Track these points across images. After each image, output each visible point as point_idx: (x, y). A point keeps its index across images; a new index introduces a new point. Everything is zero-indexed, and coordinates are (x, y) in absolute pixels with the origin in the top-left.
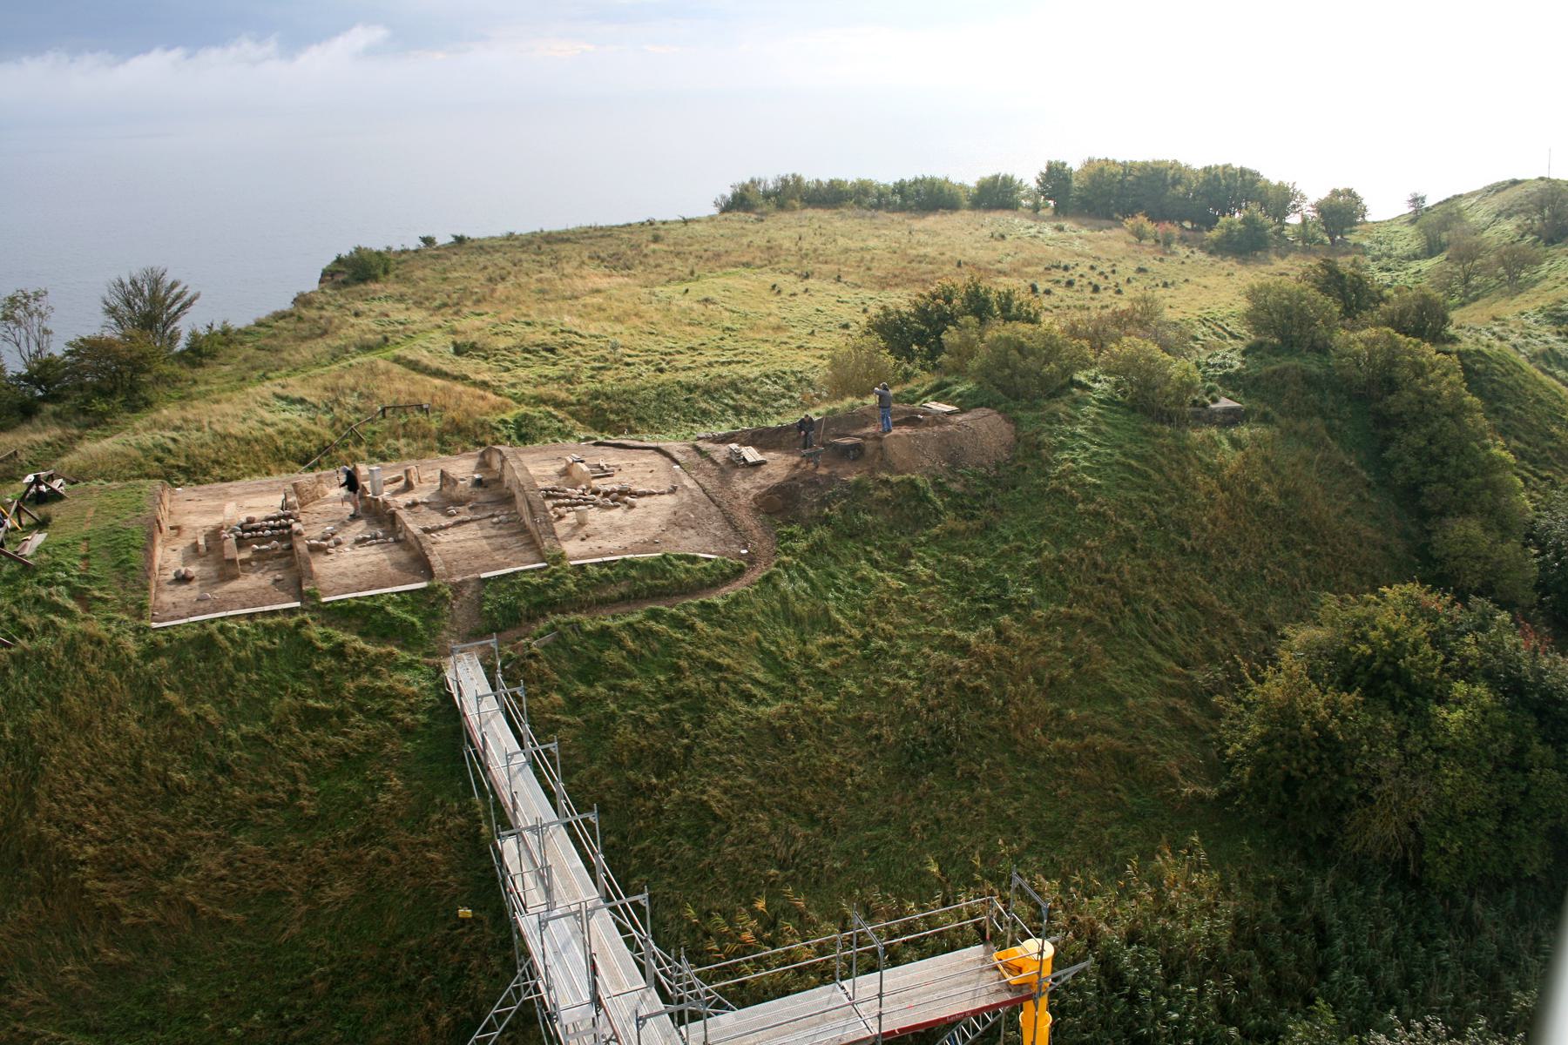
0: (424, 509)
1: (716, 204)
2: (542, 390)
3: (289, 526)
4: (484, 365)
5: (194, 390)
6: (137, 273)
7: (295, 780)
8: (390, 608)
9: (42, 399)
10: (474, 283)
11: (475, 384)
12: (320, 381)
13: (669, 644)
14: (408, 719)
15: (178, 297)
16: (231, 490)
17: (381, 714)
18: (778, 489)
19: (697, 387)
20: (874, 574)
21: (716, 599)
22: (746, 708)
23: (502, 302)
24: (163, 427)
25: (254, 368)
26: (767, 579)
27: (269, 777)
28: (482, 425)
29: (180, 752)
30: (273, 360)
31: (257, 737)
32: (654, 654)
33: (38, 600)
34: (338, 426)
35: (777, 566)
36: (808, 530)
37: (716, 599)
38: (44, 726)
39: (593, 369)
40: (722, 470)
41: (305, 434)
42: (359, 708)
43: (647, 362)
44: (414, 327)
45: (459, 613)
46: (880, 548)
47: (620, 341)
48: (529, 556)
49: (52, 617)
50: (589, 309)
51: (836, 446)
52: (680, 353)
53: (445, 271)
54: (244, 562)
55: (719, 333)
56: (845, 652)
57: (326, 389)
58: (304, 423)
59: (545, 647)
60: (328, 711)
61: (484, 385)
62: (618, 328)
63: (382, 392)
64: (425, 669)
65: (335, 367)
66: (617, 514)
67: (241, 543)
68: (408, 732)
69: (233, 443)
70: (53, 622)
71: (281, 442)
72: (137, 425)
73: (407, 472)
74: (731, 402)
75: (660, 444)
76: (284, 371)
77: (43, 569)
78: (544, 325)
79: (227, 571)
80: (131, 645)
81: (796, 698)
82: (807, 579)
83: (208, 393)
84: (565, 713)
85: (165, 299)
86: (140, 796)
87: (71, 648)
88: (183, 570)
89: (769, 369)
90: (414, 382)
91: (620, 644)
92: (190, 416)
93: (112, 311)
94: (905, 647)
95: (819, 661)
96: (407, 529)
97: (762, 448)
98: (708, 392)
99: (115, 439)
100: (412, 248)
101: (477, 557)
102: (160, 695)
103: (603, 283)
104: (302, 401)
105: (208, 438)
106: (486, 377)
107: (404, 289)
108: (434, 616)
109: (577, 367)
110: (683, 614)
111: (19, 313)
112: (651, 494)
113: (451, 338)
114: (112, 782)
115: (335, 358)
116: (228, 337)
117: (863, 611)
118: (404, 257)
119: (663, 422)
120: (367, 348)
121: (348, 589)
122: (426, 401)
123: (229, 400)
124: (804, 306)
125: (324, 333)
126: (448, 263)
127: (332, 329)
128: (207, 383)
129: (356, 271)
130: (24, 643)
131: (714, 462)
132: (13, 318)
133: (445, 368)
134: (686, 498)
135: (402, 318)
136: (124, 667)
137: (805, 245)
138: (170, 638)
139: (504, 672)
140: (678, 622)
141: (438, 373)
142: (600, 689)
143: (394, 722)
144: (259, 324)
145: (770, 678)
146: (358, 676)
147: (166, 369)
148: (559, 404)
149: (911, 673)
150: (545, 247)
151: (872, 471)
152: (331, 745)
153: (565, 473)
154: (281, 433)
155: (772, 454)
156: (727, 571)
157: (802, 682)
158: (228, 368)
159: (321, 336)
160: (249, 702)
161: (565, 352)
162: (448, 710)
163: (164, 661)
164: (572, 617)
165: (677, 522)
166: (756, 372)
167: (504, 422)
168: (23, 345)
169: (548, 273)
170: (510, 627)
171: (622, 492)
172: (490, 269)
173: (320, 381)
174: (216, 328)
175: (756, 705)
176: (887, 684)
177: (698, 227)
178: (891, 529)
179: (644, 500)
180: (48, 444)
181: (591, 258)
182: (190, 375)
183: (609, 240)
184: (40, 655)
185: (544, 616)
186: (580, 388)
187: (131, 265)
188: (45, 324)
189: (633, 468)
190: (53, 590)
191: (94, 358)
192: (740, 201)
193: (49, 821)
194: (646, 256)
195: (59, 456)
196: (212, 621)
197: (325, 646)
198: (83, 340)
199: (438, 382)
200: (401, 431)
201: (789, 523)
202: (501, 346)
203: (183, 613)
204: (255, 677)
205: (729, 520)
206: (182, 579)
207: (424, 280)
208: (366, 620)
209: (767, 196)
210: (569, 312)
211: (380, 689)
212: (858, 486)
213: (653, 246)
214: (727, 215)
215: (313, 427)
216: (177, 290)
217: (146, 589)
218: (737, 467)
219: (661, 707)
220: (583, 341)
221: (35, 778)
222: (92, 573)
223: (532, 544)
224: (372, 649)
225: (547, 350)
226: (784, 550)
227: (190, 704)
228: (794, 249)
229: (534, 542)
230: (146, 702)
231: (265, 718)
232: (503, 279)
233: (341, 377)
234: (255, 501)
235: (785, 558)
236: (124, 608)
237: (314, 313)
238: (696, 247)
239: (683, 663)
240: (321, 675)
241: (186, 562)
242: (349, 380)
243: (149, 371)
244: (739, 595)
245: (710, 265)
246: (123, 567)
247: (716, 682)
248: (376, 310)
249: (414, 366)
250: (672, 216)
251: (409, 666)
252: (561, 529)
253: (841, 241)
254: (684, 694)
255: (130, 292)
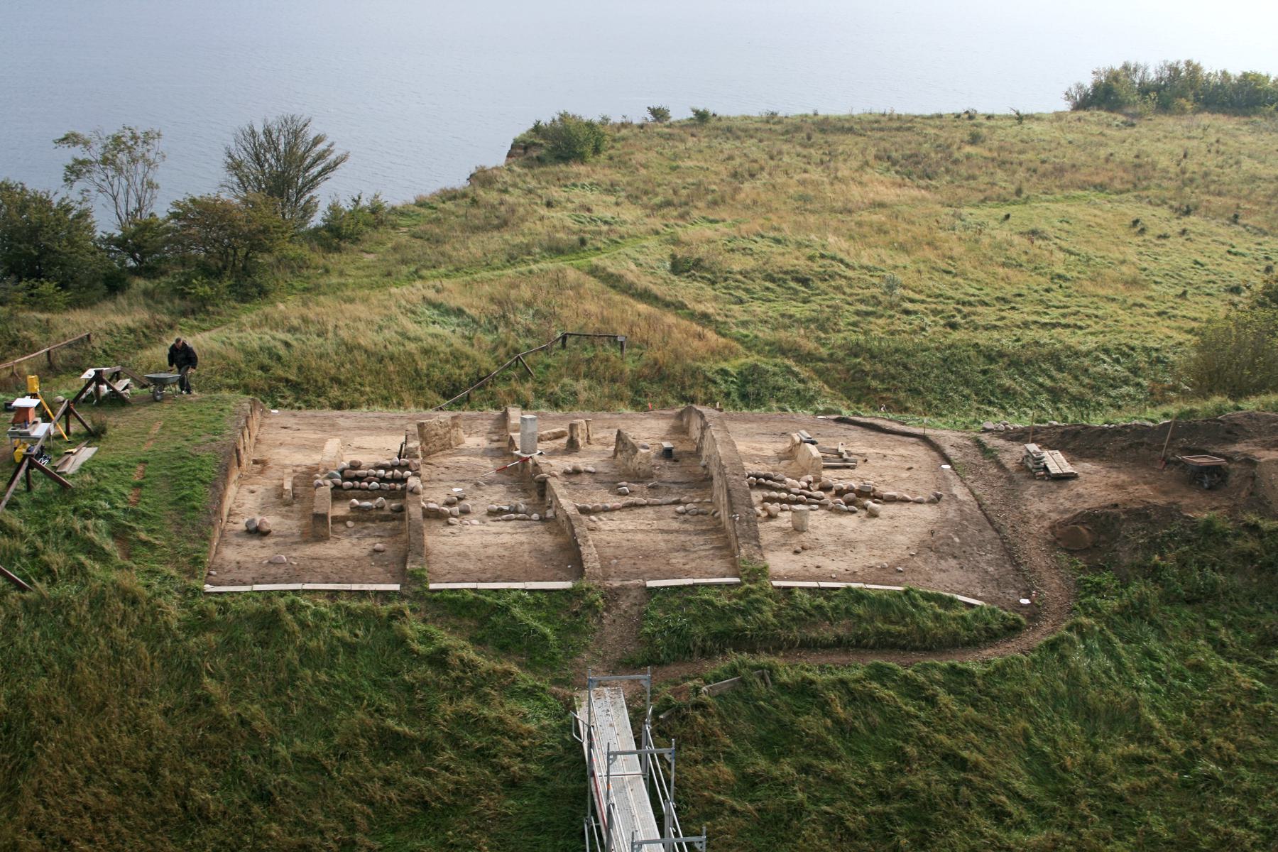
0: (587, 480)
1: (1068, 96)
2: (782, 334)
3: (404, 480)
4: (709, 291)
5: (324, 281)
6: (274, 121)
7: (353, 828)
8: (517, 611)
9: (135, 272)
10: (713, 178)
11: (692, 316)
12: (487, 288)
13: (895, 719)
14: (516, 767)
15: (321, 156)
16: (341, 422)
17: (482, 755)
18: (1089, 518)
19: (1001, 355)
20: (1215, 662)
21: (972, 662)
22: (994, 831)
23: (747, 208)
24: (276, 327)
25: (404, 262)
26: (1052, 646)
27: (319, 816)
28: (694, 373)
29: (211, 765)
30: (431, 252)
31: (313, 760)
32: (873, 730)
33: (70, 534)
34: (501, 351)
35: (1070, 629)
36: (1125, 585)
37: (972, 662)
38: (46, 701)
39: (858, 313)
40: (1010, 480)
41: (456, 357)
42: (455, 742)
43: (935, 312)
44: (623, 230)
45: (612, 631)
46: (1229, 625)
47: (900, 278)
48: (719, 565)
49: (82, 558)
50: (866, 229)
51: (1184, 466)
52: (985, 304)
53: (676, 157)
54: (338, 520)
55: (1045, 282)
56: (1154, 772)
57: (492, 300)
58: (457, 342)
59: (720, 696)
60: (413, 740)
61: (705, 318)
62: (903, 259)
63: (566, 313)
64: (552, 701)
65: (510, 272)
66: (849, 523)
67: (338, 494)
68: (513, 784)
69: (360, 357)
70: (82, 565)
71: (423, 365)
72: (244, 318)
73: (572, 427)
74: (1048, 383)
75: (928, 432)
76: (442, 270)
77: (83, 494)
78: (799, 245)
79: (318, 528)
80: (174, 612)
81: (1070, 827)
82: (1112, 655)
83: (340, 287)
84: (734, 795)
85: (303, 158)
86: (150, 815)
87: (98, 601)
88: (258, 519)
89: (1110, 340)
90: (610, 304)
91: (825, 707)
92: (311, 316)
93: (235, 167)
94: (1249, 779)
95: (1114, 778)
96: (559, 506)
97: (1075, 454)
98: (1015, 363)
99: (214, 333)
100: (637, 121)
101: (646, 557)
102: (198, 683)
103: (888, 194)
104: (459, 312)
105: (330, 347)
106: (710, 308)
107: (618, 177)
108: (575, 629)
109: (836, 309)
110: (921, 678)
111: (123, 157)
112: (906, 501)
113: (669, 249)
114: (118, 789)
115: (512, 260)
116: (377, 217)
117: (1190, 714)
118: (624, 132)
119: (946, 399)
120: (556, 250)
121: (466, 576)
122: (622, 332)
123: (365, 300)
124: (1177, 255)
125: (503, 224)
126: (681, 147)
127: (514, 220)
128: (341, 274)
129: (557, 146)
130: (42, 587)
131: (1001, 466)
132: (113, 163)
133: (655, 290)
134: (952, 513)
135: (608, 215)
136: (160, 638)
137: (1191, 166)
138: (224, 609)
139: (661, 724)
140: (913, 690)
141: (645, 296)
142: (787, 768)
143: (497, 769)
144: (421, 204)
145: (1036, 791)
146: (460, 697)
147: (293, 250)
148: (804, 358)
149: (1255, 820)
150: (817, 137)
151: (1233, 511)
152: (407, 787)
153: (790, 455)
154: (426, 352)
155: (1088, 466)
156: (995, 626)
157: (1082, 805)
158: (371, 257)
159: (498, 228)
160: (313, 710)
161: (823, 286)
162: (573, 764)
163: (212, 638)
164: (764, 659)
165: (933, 546)
166: (1091, 343)
167: (724, 372)
168: (121, 197)
169: (816, 174)
170: (676, 661)
171: (864, 493)
172: (738, 161)
173: (487, 288)
174: (364, 202)
175: (1008, 829)
176: (1216, 831)
177: (1036, 127)
178: (1252, 599)
179: (892, 509)
180: (131, 331)
181: (878, 157)
182: (322, 262)
183: (909, 136)
184: (60, 606)
185: (723, 652)
186: (837, 339)
187: (264, 113)
188: (150, 175)
189: (885, 461)
190: (90, 523)
191: (206, 226)
192: (1105, 96)
193: (30, 829)
194: (956, 162)
195: (141, 347)
196: (282, 594)
197: (422, 649)
198: (193, 201)
199: (642, 307)
200: (583, 368)
201: (1097, 568)
202: (736, 268)
203: (248, 578)
204: (324, 677)
205: (1010, 553)
206: (256, 532)
207: (645, 167)
208: (483, 621)
209: (1145, 90)
210: (836, 231)
211: (486, 720)
212: (1208, 529)
213: (968, 149)
214: (1081, 113)
215: (468, 349)
216: (321, 147)
217: (206, 538)
218: (1034, 477)
219: (870, 808)
220: (849, 273)
221: (23, 768)
222: (141, 508)
223: (726, 549)
224: (485, 664)
225: (797, 280)
226: (1084, 606)
227: (234, 702)
228: (1173, 170)
229: (728, 546)
230: (179, 690)
231: (328, 734)
232: (752, 176)
233: (514, 286)
234: (368, 440)
235: (1084, 620)
236: (173, 560)
237: (491, 196)
238: (1030, 155)
239: (911, 750)
240: (410, 688)
241: (263, 509)
242: (526, 292)
243: (269, 251)
244: (1007, 664)
245: (1047, 182)
246: (183, 504)
247: (956, 784)
248: (579, 197)
249: (614, 282)
250: (1001, 108)
251: (530, 693)
252: (768, 533)
253: (1247, 164)
254: (906, 794)
255: (261, 145)
